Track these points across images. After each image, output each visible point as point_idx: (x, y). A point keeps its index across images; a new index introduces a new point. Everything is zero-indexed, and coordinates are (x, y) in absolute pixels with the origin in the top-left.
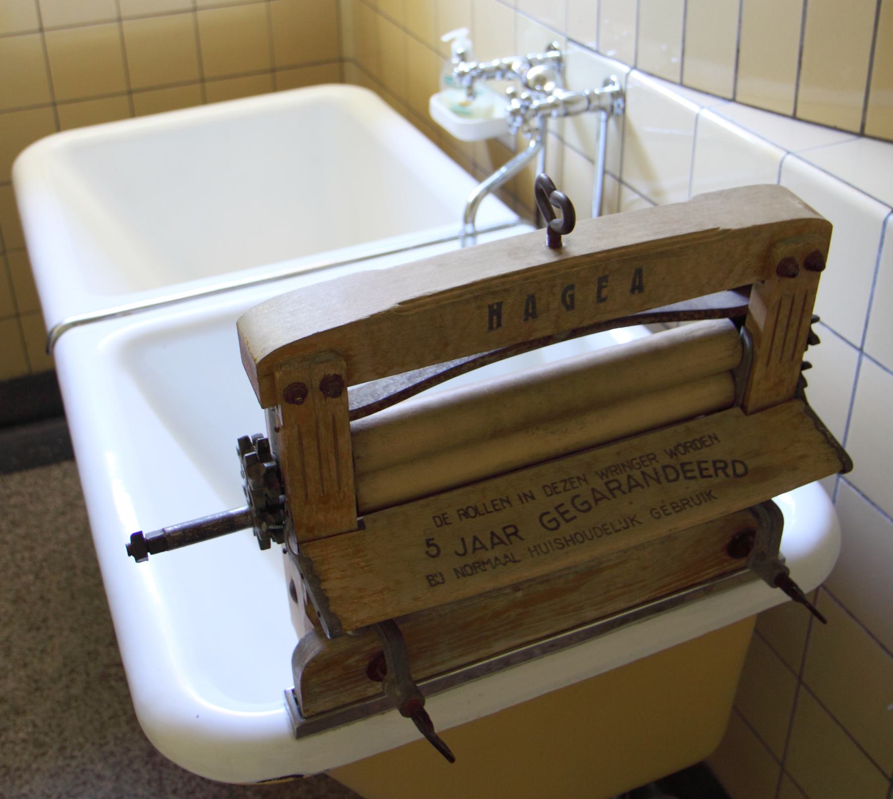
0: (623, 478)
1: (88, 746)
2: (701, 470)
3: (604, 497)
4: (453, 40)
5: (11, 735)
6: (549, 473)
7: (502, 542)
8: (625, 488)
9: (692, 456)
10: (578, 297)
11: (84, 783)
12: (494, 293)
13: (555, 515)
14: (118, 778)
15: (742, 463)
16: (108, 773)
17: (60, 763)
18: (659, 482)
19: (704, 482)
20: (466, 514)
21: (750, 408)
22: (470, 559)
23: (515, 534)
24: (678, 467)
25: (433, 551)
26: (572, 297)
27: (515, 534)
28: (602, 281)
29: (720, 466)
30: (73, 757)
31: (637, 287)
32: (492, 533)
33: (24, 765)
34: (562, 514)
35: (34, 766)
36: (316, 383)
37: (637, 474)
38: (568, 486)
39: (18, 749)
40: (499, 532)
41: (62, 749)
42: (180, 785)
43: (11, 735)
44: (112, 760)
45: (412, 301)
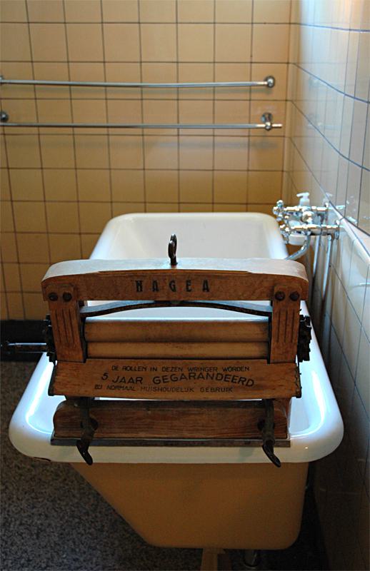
0: (198, 373)
1: (76, 482)
2: (233, 379)
3: (186, 378)
4: (301, 197)
5: (48, 468)
6: (168, 363)
7: (133, 382)
8: (196, 377)
9: (233, 373)
10: (177, 286)
11: (67, 497)
12: (138, 276)
13: (161, 379)
14: (81, 499)
15: (252, 381)
16: (78, 496)
17: (62, 485)
18: (212, 379)
19: (231, 384)
20: (126, 369)
21: (271, 361)
22: (116, 384)
23: (140, 381)
24: (224, 376)
25: (105, 377)
26: (174, 286)
27: (140, 381)
28: (188, 283)
29: (242, 380)
30: (67, 485)
31: (206, 289)
32: (132, 378)
33: (47, 481)
34: (163, 379)
35: (51, 483)
36: (61, 295)
37: (205, 374)
38: (174, 370)
39: (48, 474)
40: (134, 379)
41: (65, 480)
42: (104, 510)
43: (48, 468)
44: (82, 491)
45: (104, 272)
